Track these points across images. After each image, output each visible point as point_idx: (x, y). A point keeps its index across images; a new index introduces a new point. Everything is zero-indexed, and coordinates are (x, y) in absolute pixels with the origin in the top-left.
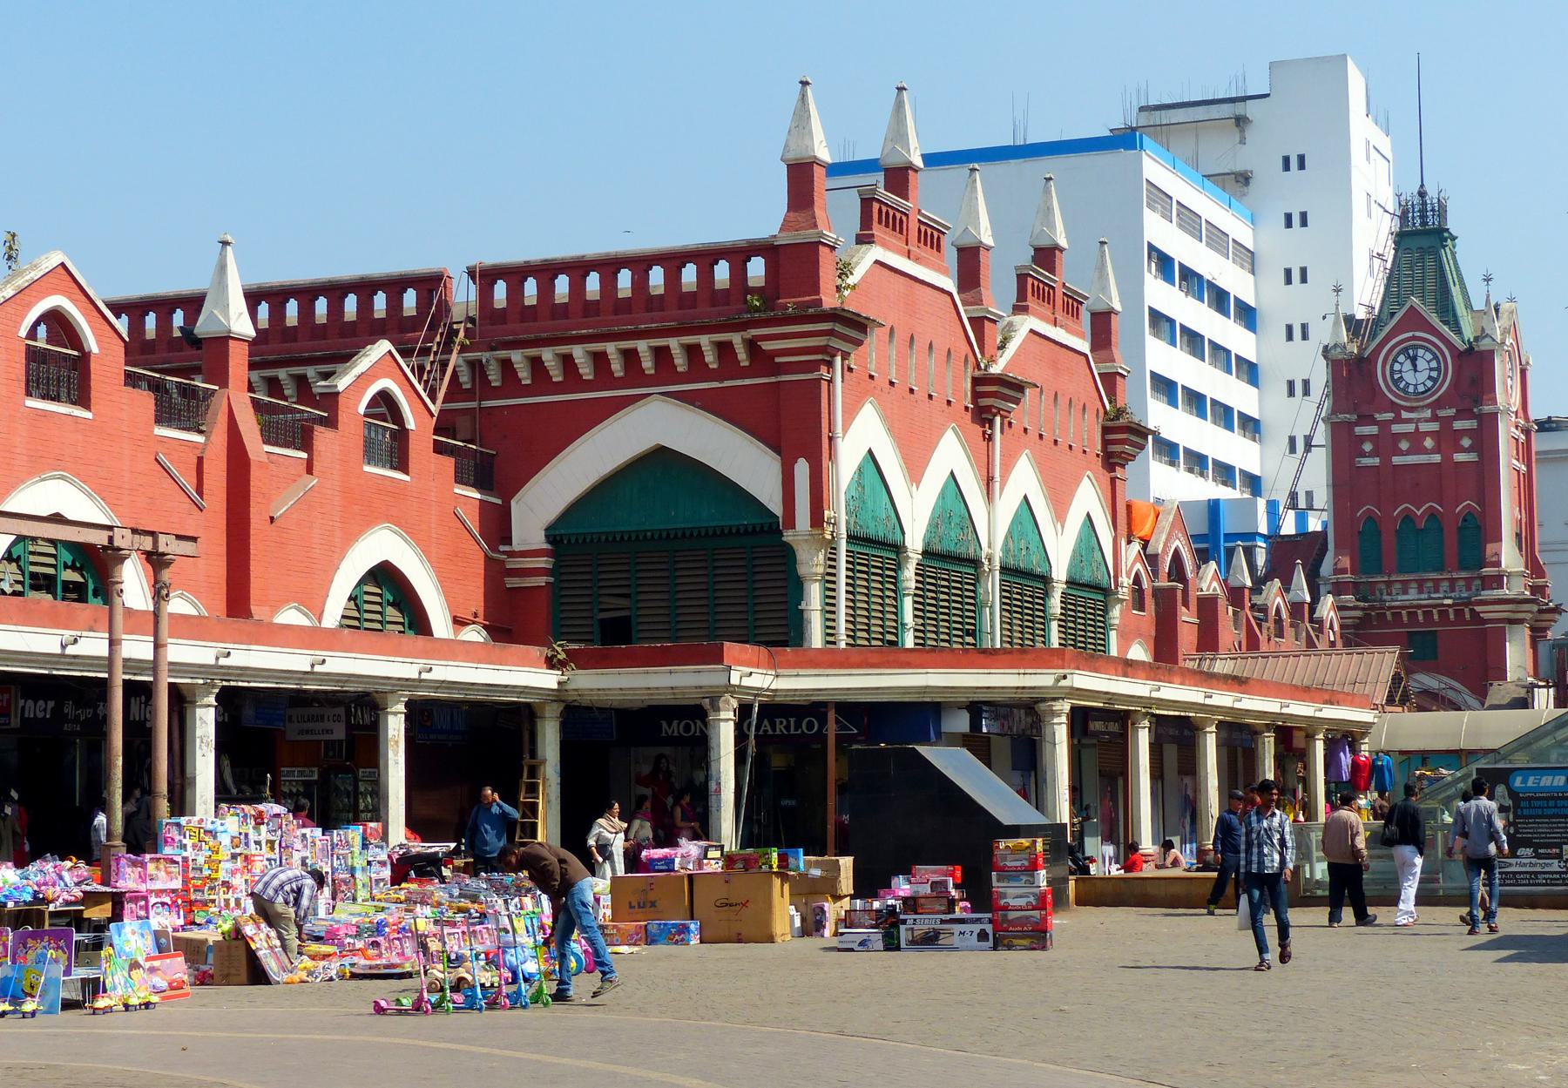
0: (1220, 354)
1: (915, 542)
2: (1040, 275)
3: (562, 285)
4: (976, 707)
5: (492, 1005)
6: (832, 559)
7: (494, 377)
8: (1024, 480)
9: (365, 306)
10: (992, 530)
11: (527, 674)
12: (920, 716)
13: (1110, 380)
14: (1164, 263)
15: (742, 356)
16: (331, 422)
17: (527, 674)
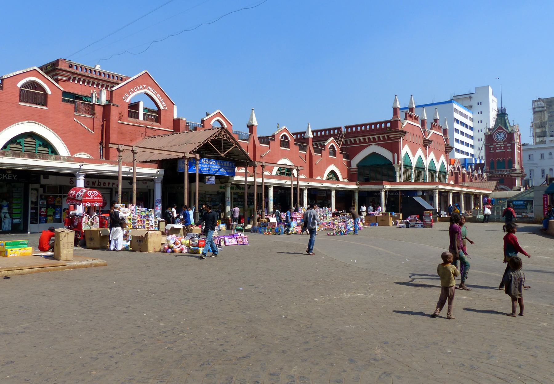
0: (467, 135)
1: (414, 166)
2: (435, 124)
3: (368, 127)
4: (423, 191)
5: (345, 234)
6: (400, 168)
7: (349, 142)
8: (432, 156)
9: (330, 132)
10: (427, 163)
11: (353, 186)
12: (414, 192)
13: (446, 140)
14: (457, 121)
15: (386, 138)
16: (324, 150)
17: (353, 186)
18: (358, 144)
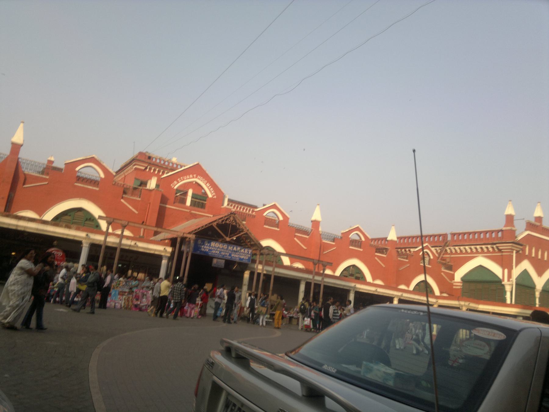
18: (459, 254)
